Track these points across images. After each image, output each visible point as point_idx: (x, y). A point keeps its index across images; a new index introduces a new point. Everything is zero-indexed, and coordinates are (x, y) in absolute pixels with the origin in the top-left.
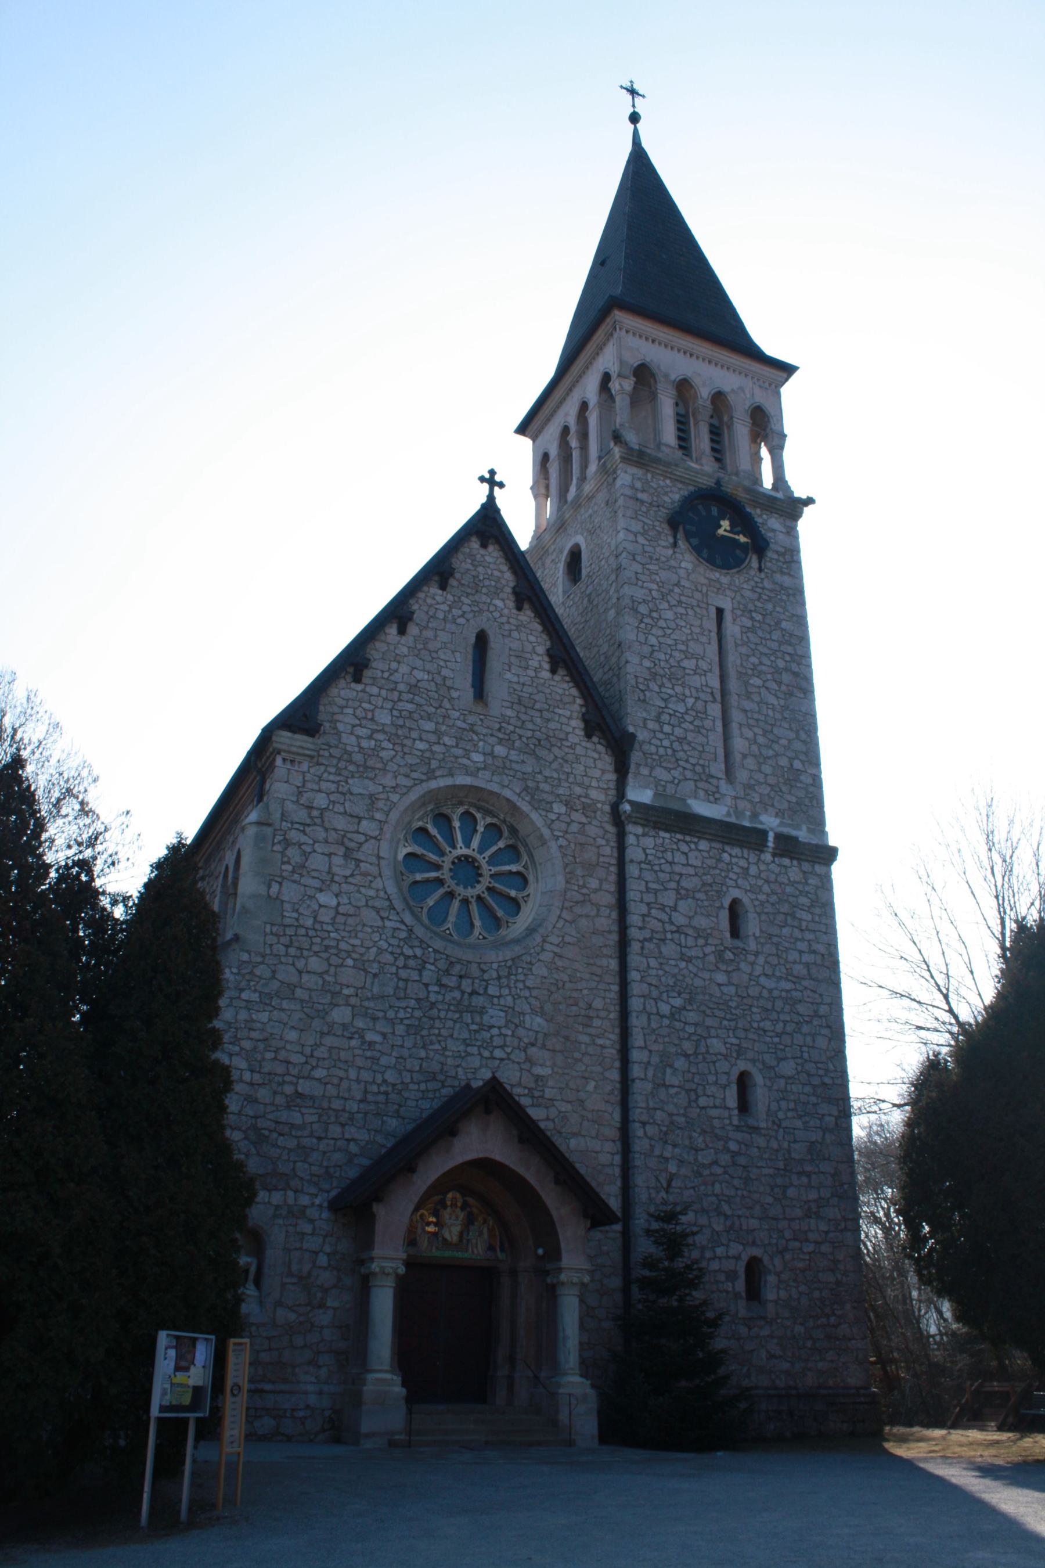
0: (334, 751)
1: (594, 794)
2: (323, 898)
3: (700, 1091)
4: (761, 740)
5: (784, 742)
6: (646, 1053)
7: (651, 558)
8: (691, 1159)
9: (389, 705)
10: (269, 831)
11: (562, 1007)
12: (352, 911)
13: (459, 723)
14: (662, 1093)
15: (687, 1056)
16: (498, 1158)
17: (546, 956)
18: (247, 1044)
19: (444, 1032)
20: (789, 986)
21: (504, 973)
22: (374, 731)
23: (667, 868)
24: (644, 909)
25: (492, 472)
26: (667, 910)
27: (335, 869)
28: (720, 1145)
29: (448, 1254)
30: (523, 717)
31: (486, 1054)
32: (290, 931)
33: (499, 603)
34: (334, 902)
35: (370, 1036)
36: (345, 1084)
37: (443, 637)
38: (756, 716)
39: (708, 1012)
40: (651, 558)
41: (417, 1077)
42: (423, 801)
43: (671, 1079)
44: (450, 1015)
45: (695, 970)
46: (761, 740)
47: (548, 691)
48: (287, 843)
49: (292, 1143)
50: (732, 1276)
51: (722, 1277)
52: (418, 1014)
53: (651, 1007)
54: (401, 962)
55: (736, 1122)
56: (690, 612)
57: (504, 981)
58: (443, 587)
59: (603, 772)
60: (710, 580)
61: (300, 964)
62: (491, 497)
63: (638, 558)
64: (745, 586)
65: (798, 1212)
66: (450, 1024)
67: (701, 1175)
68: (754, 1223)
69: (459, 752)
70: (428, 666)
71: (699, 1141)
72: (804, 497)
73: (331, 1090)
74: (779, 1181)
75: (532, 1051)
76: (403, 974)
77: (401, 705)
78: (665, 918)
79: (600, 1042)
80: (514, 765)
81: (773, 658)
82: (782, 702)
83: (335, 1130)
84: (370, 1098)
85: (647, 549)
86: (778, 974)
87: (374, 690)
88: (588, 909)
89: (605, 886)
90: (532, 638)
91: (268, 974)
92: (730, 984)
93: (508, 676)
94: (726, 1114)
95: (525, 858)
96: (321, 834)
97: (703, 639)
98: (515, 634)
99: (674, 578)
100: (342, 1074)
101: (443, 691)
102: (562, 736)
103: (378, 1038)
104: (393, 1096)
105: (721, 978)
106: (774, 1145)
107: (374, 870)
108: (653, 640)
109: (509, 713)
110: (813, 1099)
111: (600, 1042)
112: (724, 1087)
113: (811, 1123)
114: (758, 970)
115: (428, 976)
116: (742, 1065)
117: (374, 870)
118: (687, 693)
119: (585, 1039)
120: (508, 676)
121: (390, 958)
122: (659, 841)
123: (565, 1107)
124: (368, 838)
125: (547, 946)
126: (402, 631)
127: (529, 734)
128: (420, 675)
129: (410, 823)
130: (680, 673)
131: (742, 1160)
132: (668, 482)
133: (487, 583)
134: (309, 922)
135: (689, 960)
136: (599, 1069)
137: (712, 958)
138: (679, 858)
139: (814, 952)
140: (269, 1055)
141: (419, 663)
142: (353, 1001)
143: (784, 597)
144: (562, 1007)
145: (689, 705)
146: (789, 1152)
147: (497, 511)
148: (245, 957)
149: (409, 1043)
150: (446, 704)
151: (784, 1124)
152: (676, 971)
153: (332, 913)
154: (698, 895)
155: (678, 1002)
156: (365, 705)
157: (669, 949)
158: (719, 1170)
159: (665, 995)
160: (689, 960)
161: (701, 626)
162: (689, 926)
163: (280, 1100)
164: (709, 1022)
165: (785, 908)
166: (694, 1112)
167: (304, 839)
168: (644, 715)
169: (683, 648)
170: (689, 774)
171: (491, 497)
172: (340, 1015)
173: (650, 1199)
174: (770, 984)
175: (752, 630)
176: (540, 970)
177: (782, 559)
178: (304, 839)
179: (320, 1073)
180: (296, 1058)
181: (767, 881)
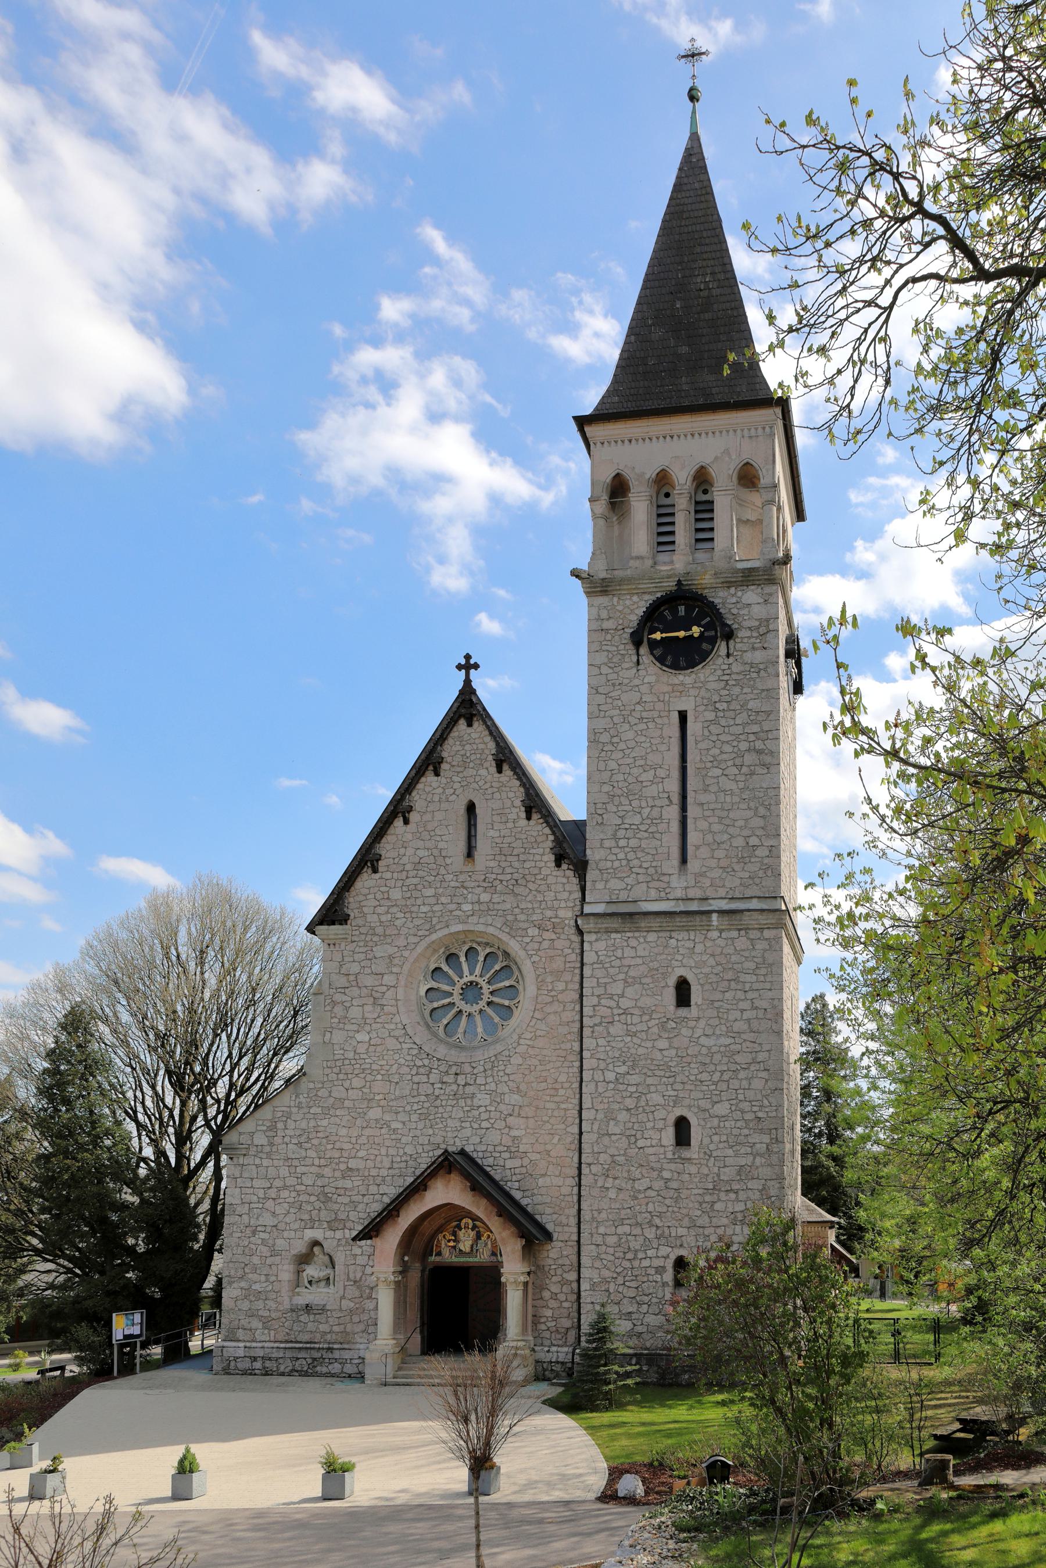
0: (363, 930)
1: (562, 913)
2: (360, 1037)
3: (639, 1136)
4: (716, 828)
5: (741, 823)
6: (593, 1112)
7: (614, 685)
8: (629, 1187)
9: (400, 884)
10: (322, 997)
11: (534, 1085)
12: (379, 1041)
13: (453, 884)
14: (606, 1140)
15: (628, 1110)
16: (457, 1202)
17: (521, 1049)
18: (315, 1142)
19: (445, 1115)
20: (729, 1041)
21: (488, 1066)
22: (389, 907)
23: (617, 963)
24: (595, 1001)
25: (468, 657)
26: (616, 998)
27: (367, 1015)
28: (655, 1174)
29: (462, 1260)
30: (503, 864)
31: (476, 1126)
32: (339, 1063)
33: (483, 772)
34: (367, 1038)
35: (394, 1125)
36: (379, 1158)
37: (439, 816)
38: (712, 806)
39: (649, 1073)
40: (614, 685)
41: (427, 1148)
42: (433, 948)
43: (613, 1128)
44: (450, 1102)
45: (639, 1042)
46: (716, 828)
47: (524, 836)
48: (334, 1003)
49: (346, 1200)
50: (660, 1270)
51: (652, 1271)
52: (426, 1105)
53: (598, 1076)
54: (414, 1072)
55: (670, 1155)
56: (651, 725)
57: (489, 1072)
58: (437, 774)
59: (570, 892)
60: (673, 685)
61: (347, 1084)
62: (468, 682)
63: (600, 690)
64: (711, 678)
65: (725, 1221)
66: (449, 1108)
67: (637, 1198)
68: (682, 1231)
69: (453, 907)
70: (429, 844)
71: (637, 1174)
72: (578, 582)
73: (370, 1164)
74: (708, 1198)
75: (510, 1120)
76: (416, 1079)
77: (408, 882)
78: (613, 1004)
79: (563, 1106)
80: (496, 906)
81: (735, 743)
82: (741, 785)
83: (373, 1189)
84: (395, 1165)
85: (610, 677)
86: (718, 1032)
87: (388, 875)
88: (556, 1007)
89: (570, 986)
90: (511, 795)
91: (326, 1094)
92: (671, 1047)
93: (492, 833)
94: (662, 1150)
95: (516, 973)
96: (355, 992)
97: (663, 748)
98: (497, 795)
99: (635, 697)
100: (376, 1152)
101: (440, 861)
102: (536, 871)
103: (400, 1126)
104: (411, 1163)
105: (662, 1044)
106: (705, 1171)
107: (393, 1010)
108: (613, 765)
109: (492, 864)
110: (746, 1132)
111: (563, 1106)
112: (660, 1130)
113: (742, 1151)
114: (699, 1032)
115: (434, 1077)
116: (678, 1112)
117: (393, 1010)
118: (644, 804)
119: (552, 1106)
120: (492, 833)
121: (407, 1070)
122: (610, 942)
123: (534, 1157)
124: (389, 987)
125: (522, 1041)
126: (406, 822)
127: (509, 877)
128: (421, 853)
129: (427, 966)
130: (636, 787)
131: (674, 1185)
132: (635, 598)
133: (473, 757)
134: (351, 1055)
135: (635, 1034)
136: (563, 1126)
137: (655, 1030)
138: (629, 952)
139: (756, 1008)
140: (330, 1147)
141: (420, 844)
142: (382, 1103)
143: (755, 675)
144: (534, 1085)
145: (645, 816)
146: (718, 1175)
147: (473, 692)
148: (311, 1085)
149: (421, 1125)
150: (443, 871)
151: (715, 1154)
152: (622, 1045)
153: (366, 1046)
154: (644, 981)
155: (623, 1069)
156: (383, 889)
157: (616, 1029)
158: (653, 1194)
159: (611, 1067)
160: (635, 1034)
161: (661, 737)
162: (636, 1006)
163: (338, 1174)
164: (649, 1081)
165: (730, 975)
166: (633, 1152)
167: (345, 998)
168: (602, 836)
169: (642, 762)
170: (641, 878)
171: (468, 682)
172: (374, 1113)
173: (593, 1218)
174: (711, 1042)
175: (715, 722)
176: (516, 1060)
177: (755, 634)
178: (345, 998)
179: (361, 1154)
180: (346, 1146)
181: (713, 955)
